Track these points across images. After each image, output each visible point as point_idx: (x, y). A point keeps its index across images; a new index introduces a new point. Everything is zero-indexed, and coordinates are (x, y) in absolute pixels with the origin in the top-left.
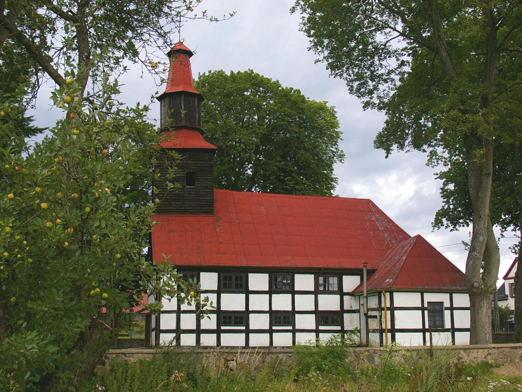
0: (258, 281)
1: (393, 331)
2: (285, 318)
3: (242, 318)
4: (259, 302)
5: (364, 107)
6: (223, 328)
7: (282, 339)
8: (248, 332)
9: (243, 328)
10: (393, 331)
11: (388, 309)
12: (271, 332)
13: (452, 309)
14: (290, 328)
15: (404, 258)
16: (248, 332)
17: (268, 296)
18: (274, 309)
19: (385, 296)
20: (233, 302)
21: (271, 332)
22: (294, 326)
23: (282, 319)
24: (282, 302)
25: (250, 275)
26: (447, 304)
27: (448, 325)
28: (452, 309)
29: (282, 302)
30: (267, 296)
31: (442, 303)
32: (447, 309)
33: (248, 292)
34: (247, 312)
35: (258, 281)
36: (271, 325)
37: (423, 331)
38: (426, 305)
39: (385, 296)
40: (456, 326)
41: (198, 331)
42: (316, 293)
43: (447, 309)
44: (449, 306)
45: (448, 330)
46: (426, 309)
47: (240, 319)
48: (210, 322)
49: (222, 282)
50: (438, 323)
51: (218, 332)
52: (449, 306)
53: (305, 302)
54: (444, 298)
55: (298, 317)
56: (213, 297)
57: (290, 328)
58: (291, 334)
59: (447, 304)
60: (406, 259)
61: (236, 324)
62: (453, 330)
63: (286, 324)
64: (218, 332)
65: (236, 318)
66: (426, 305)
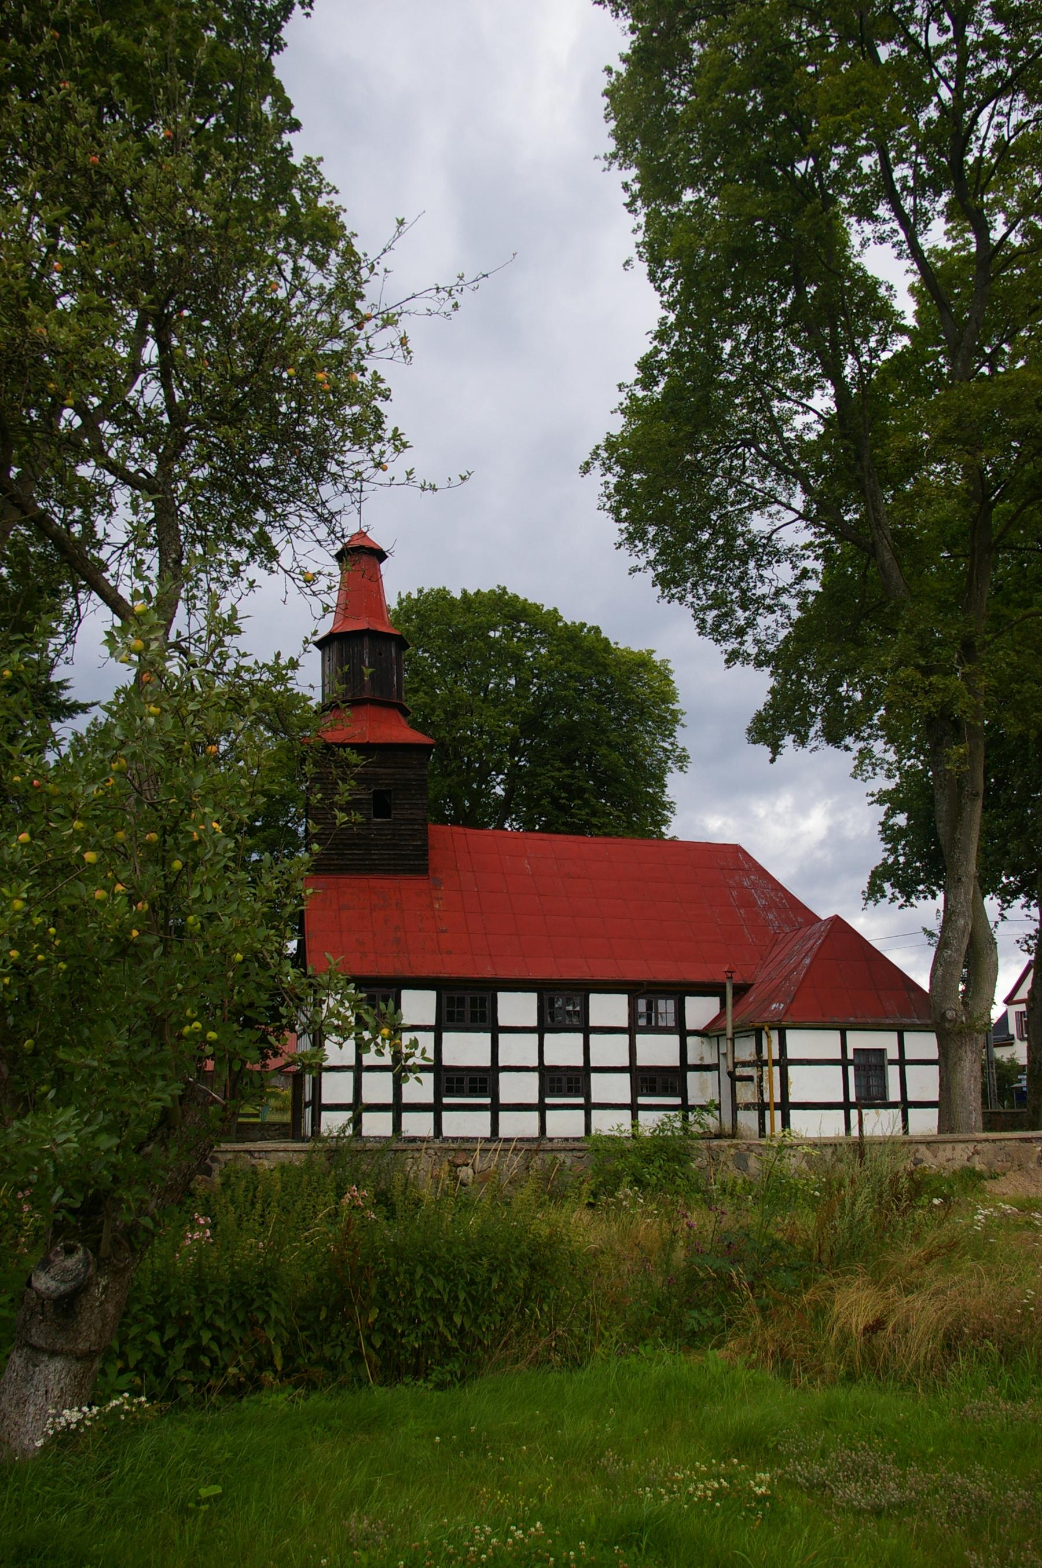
0: (517, 1008)
1: (786, 1106)
2: (570, 1081)
3: (483, 1081)
4: (517, 1050)
5: (727, 661)
6: (446, 1100)
7: (565, 1123)
8: (496, 1108)
9: (487, 1101)
10: (786, 1106)
11: (775, 1063)
12: (541, 1108)
13: (902, 1062)
14: (581, 1100)
15: (807, 961)
16: (496, 1108)
17: (536, 1036)
18: (547, 1063)
19: (768, 1037)
20: (466, 1049)
21: (541, 1108)
22: (588, 1096)
23: (565, 1083)
24: (564, 1050)
25: (501, 996)
26: (893, 1054)
27: (894, 1095)
28: (902, 1062)
29: (564, 1050)
30: (535, 1037)
31: (882, 1051)
32: (892, 1062)
33: (496, 1030)
34: (495, 1068)
35: (517, 1008)
36: (542, 1094)
37: (846, 1106)
38: (850, 1056)
39: (768, 1037)
40: (911, 1097)
41: (398, 1108)
42: (632, 1031)
43: (892, 1062)
44: (896, 1057)
45: (894, 1105)
46: (851, 1063)
47: (478, 1084)
48: (420, 1089)
49: (445, 1010)
50: (874, 1091)
51: (437, 1108)
52: (896, 1057)
53: (609, 1050)
54: (886, 1041)
55: (692, 1078)
56: (427, 1040)
57: (581, 1100)
58: (582, 1113)
59: (893, 1054)
60: (811, 963)
61: (473, 1092)
62: (905, 1105)
63: (571, 1092)
64: (437, 1108)
65: (473, 1081)
66: (850, 1056)
